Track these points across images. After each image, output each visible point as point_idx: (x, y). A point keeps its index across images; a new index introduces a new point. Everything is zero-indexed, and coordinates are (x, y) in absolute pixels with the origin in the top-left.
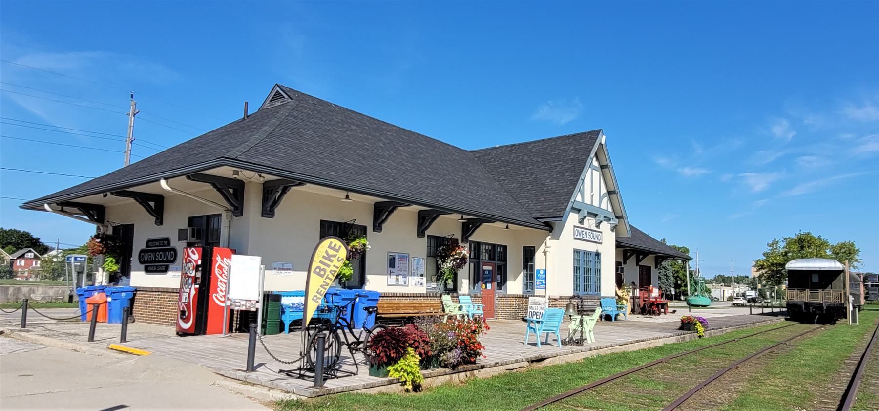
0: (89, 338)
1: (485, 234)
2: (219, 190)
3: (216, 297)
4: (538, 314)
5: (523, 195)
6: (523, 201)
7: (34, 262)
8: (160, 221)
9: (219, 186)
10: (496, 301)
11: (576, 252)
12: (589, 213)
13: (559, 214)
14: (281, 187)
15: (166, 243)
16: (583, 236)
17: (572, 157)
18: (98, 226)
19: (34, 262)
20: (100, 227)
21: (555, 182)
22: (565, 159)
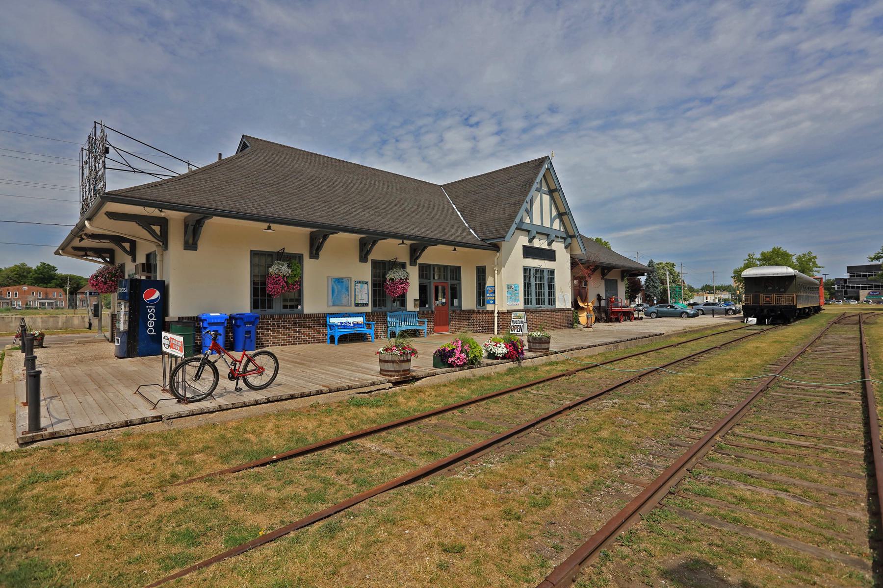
1: (432, 256)
11: (526, 270)
12: (538, 233)
14: (372, 241)
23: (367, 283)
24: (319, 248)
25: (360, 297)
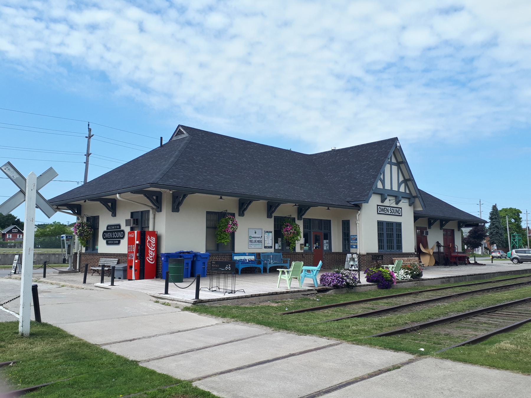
0: (84, 282)
1: (312, 214)
2: (148, 198)
3: (148, 259)
4: (355, 265)
7: (18, 235)
8: (114, 215)
9: (148, 196)
10: (324, 257)
11: (380, 223)
15: (118, 227)
16: (386, 211)
17: (375, 158)
19: (18, 235)
20: (80, 218)
22: (371, 159)
23: (271, 232)
24: (180, 204)
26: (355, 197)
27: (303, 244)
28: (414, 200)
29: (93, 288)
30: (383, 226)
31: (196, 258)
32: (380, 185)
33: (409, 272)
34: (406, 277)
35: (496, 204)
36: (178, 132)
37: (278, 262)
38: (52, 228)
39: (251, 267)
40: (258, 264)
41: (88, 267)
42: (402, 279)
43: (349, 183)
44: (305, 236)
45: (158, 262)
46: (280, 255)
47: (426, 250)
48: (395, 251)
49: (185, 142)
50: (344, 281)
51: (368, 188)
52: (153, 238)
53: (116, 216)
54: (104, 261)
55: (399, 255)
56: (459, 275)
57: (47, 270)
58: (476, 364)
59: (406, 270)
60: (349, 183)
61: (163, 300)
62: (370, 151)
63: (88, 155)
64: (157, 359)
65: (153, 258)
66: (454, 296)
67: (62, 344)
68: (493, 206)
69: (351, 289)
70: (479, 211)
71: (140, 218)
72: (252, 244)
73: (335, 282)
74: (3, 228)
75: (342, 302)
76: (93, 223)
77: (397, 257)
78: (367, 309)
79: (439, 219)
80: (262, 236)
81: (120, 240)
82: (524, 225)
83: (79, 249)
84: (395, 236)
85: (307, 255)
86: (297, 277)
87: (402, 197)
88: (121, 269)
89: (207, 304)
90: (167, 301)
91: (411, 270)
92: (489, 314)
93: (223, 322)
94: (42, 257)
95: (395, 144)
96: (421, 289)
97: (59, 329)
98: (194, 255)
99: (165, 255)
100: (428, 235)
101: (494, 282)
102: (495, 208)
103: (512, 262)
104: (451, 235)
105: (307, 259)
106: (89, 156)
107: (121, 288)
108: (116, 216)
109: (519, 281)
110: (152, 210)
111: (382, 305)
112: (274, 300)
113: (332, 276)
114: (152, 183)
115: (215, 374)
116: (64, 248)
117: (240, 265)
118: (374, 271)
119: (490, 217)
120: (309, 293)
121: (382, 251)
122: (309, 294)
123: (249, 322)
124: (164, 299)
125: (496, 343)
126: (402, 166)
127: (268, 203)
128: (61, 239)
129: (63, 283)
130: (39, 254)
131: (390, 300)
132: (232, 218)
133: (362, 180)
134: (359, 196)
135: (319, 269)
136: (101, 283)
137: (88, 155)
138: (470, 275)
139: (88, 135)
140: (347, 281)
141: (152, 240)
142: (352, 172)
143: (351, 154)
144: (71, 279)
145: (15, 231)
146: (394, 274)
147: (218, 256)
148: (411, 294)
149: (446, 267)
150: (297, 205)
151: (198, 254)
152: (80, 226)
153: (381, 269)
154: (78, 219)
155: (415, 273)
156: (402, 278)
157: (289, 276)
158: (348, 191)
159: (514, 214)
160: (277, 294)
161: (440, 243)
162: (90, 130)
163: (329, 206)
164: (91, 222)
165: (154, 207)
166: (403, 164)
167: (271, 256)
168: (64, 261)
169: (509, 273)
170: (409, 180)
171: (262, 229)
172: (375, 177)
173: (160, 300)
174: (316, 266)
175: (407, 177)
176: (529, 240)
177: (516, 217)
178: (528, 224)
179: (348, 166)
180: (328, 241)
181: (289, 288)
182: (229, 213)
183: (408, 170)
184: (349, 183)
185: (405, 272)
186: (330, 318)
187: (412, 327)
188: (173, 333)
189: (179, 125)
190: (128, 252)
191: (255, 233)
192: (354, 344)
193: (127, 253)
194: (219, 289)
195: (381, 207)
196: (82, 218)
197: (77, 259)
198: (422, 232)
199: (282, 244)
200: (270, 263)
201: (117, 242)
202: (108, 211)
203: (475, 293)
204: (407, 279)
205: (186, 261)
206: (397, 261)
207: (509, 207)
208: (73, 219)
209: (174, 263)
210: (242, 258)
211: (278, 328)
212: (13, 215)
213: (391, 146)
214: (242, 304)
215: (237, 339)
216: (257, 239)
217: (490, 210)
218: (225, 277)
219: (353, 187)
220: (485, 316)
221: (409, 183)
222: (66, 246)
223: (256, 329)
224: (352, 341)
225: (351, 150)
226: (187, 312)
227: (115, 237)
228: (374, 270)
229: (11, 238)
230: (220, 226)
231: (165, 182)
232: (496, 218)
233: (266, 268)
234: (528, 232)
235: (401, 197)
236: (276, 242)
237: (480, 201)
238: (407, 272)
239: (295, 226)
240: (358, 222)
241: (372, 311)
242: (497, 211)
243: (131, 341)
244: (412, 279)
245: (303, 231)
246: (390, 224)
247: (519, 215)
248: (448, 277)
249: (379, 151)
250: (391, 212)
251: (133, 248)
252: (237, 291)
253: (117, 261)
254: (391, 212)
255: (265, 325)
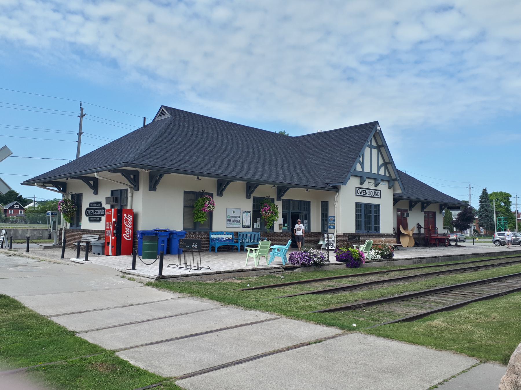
2: (125, 176)
3: (125, 236)
4: (332, 245)
5: (322, 168)
6: (321, 172)
8: (96, 193)
13: (342, 181)
15: (99, 205)
16: (364, 193)
17: (356, 141)
18: (63, 194)
20: (65, 195)
21: (343, 159)
23: (250, 212)
25: (245, 222)
26: (333, 179)
27: (282, 224)
28: (394, 183)
29: (68, 263)
30: (361, 208)
31: (172, 236)
32: (359, 168)
33: (380, 252)
34: (377, 257)
35: (486, 188)
36: (161, 113)
37: (255, 241)
38: (52, 205)
39: (229, 245)
40: (235, 242)
41: (66, 242)
42: (373, 259)
43: (329, 165)
44: (283, 216)
45: (135, 240)
46: (258, 235)
47: (406, 231)
48: (373, 231)
49: (167, 122)
50: (312, 259)
51: (347, 171)
52: (130, 216)
53: (97, 194)
54: (86, 237)
55: (377, 235)
56: (432, 256)
57: (30, 245)
58: (397, 339)
59: (377, 251)
60: (328, 166)
61: (129, 276)
62: (351, 134)
63: (80, 134)
64: (96, 330)
65: (129, 235)
66: (419, 276)
67: (12, 315)
68: (483, 189)
69: (318, 267)
70: (469, 194)
71: (119, 196)
72: (230, 223)
73: (303, 261)
74: (5, 203)
75: (306, 280)
76: (77, 200)
77: (374, 238)
78: (328, 286)
79: (420, 202)
80: (240, 216)
81: (101, 217)
82: (513, 209)
83: (63, 226)
84: (373, 217)
85: (286, 234)
86: (264, 255)
87: (382, 180)
88: (100, 245)
89: (170, 280)
90: (132, 276)
91: (381, 250)
92: (445, 294)
93: (179, 297)
94: (35, 233)
95: (375, 127)
96: (390, 268)
97: (14, 301)
98: (170, 233)
99: (141, 233)
100: (408, 217)
101: (466, 264)
102: (485, 192)
103: (494, 245)
104: (432, 218)
105: (285, 238)
106: (81, 135)
107: (93, 263)
108: (97, 194)
109: (491, 263)
110: (130, 189)
111: (344, 283)
112: (240, 277)
113: (300, 255)
114: (126, 163)
115: (143, 345)
116: (49, 223)
117: (217, 243)
118: (344, 251)
119: (480, 200)
120: (275, 270)
121: (360, 232)
122: (275, 272)
123: (203, 298)
124: (130, 275)
125: (428, 321)
126: (382, 149)
127: (247, 183)
128: (47, 215)
129: (42, 258)
130: (32, 229)
131: (354, 279)
132: (209, 198)
133: (342, 162)
134: (337, 178)
135: (287, 248)
136: (77, 258)
137: (80, 134)
138: (444, 256)
139: (80, 114)
140: (314, 260)
141: (129, 217)
142: (333, 155)
143: (333, 137)
144: (53, 254)
145: (16, 207)
146: (363, 254)
147: (196, 234)
148: (378, 273)
149: (426, 248)
150: (275, 186)
151: (174, 232)
152: (64, 203)
153: (350, 249)
154: (63, 196)
155: (385, 253)
156: (372, 258)
157: (256, 254)
158: (328, 173)
159: (504, 198)
160: (242, 271)
161: (420, 225)
162: (82, 109)
163: (308, 187)
164: (76, 199)
165: (132, 186)
166: (383, 147)
167: (249, 235)
168: (50, 237)
169: (484, 254)
170: (389, 163)
171: (240, 209)
172: (354, 160)
173: (127, 276)
174: (285, 245)
175: (387, 160)
176: (518, 223)
177: (506, 200)
178: (517, 207)
179: (329, 149)
180: (307, 221)
181: (256, 266)
182: (207, 193)
183: (388, 154)
184: (329, 165)
185: (376, 253)
186: (285, 295)
187: (359, 304)
188: (126, 306)
189: (162, 106)
190: (106, 229)
191: (234, 212)
192: (291, 319)
193: (105, 230)
194: (187, 265)
195: (359, 189)
196: (67, 195)
197: (62, 235)
198: (402, 214)
199: (261, 224)
200: (248, 242)
201: (98, 219)
202: (91, 189)
203: (441, 274)
204: (377, 259)
205: (161, 239)
206: (367, 242)
207: (499, 191)
208: (59, 196)
209: (148, 240)
210: (220, 236)
211: (227, 302)
212: (15, 191)
213: (372, 129)
214: (206, 280)
215: (183, 313)
216: (235, 219)
217: (480, 194)
218: (199, 254)
219: (332, 170)
220: (438, 295)
221: (389, 166)
222: (51, 222)
223: (207, 304)
224: (291, 316)
225: (333, 133)
226: (149, 287)
227: (97, 214)
228: (343, 250)
229: (13, 213)
230: (197, 206)
231: (140, 162)
232: (485, 202)
233: (243, 247)
234: (517, 216)
235: (380, 180)
236: (254, 221)
237: (470, 185)
238: (377, 252)
239: (273, 207)
240: (336, 203)
241: (331, 288)
242: (487, 194)
243: (81, 313)
244: (382, 259)
245: (282, 212)
246: (368, 206)
247: (509, 199)
248: (420, 258)
249: (360, 134)
250: (369, 194)
251: (110, 225)
252: (203, 268)
253: (98, 238)
254: (369, 194)
255: (217, 301)
